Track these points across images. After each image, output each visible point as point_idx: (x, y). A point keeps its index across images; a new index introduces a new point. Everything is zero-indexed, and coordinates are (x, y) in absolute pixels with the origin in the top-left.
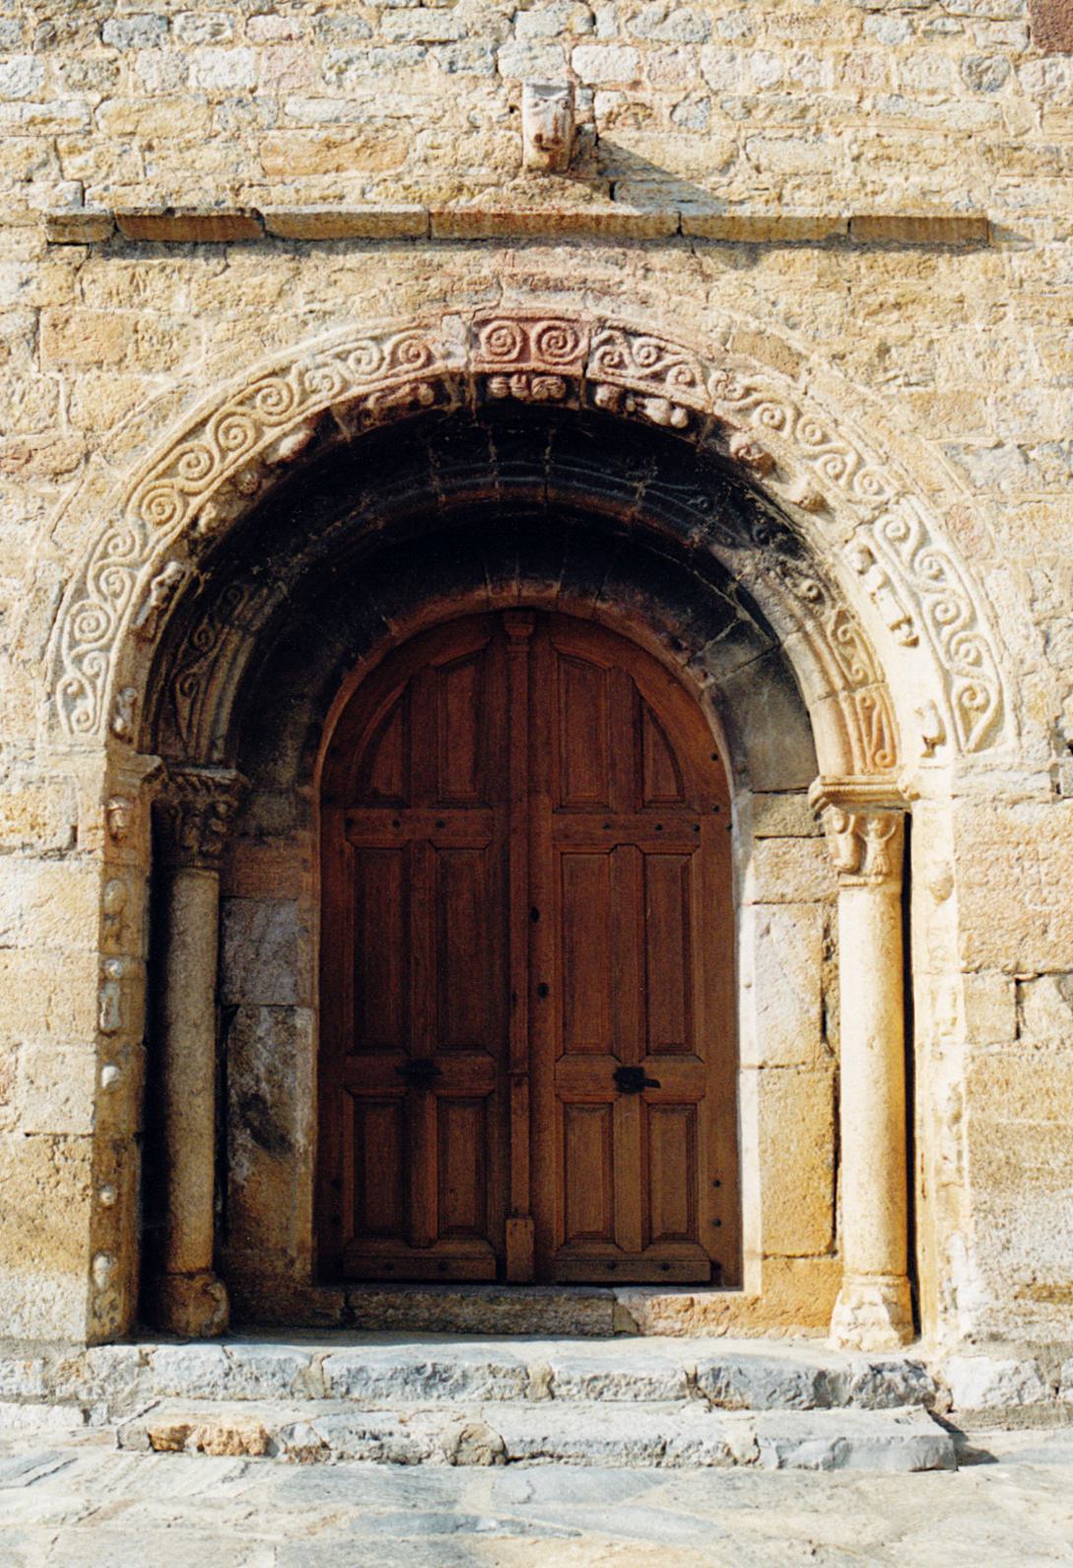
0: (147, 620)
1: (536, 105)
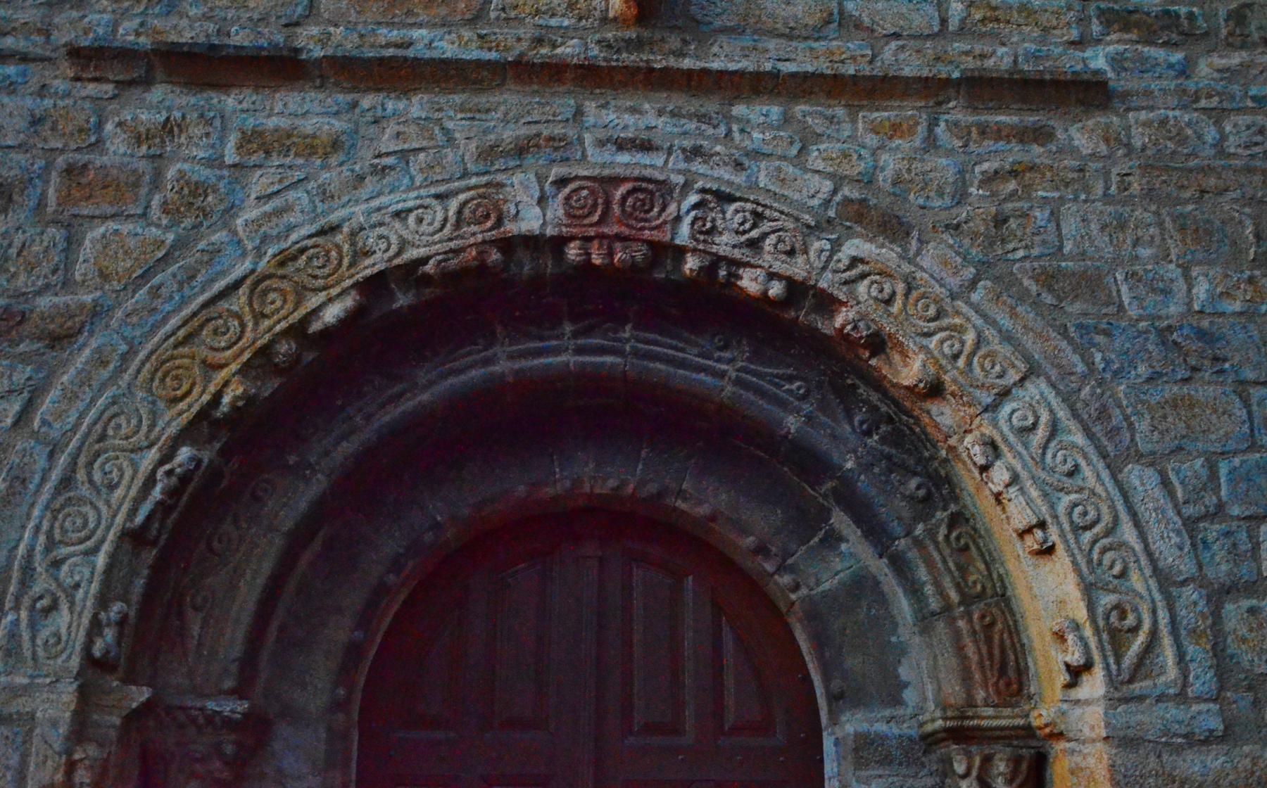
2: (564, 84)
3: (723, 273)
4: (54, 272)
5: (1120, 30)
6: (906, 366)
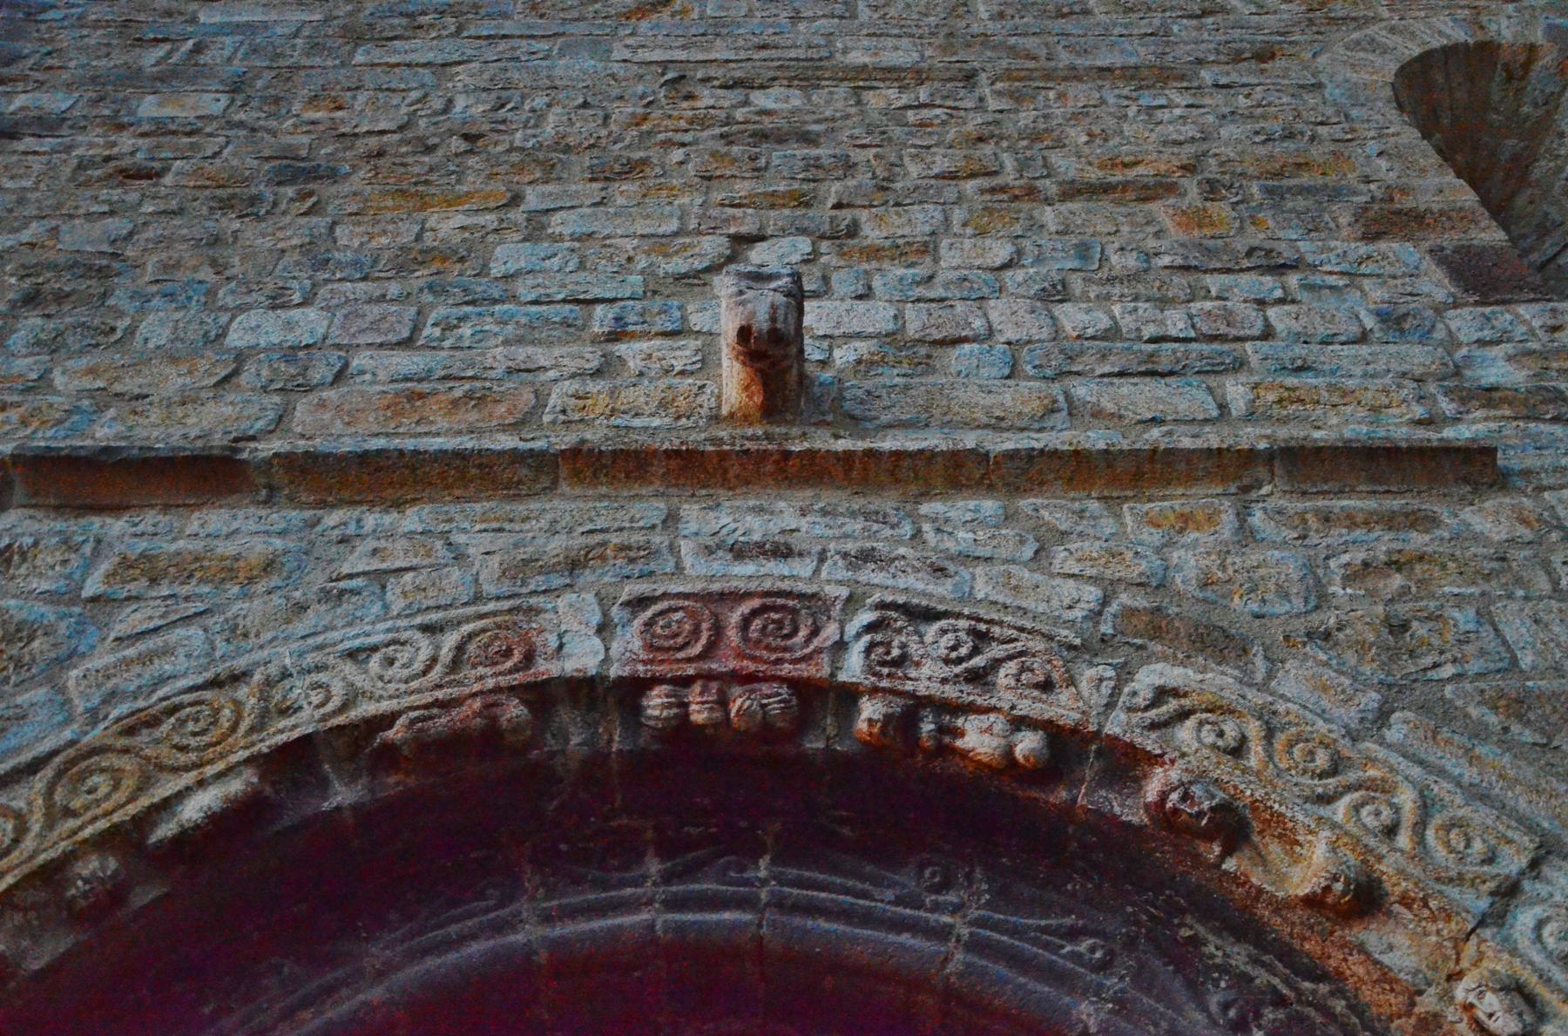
1: (741, 293)
2: (651, 483)
3: (927, 727)
5: (1484, 407)
6: (1296, 860)
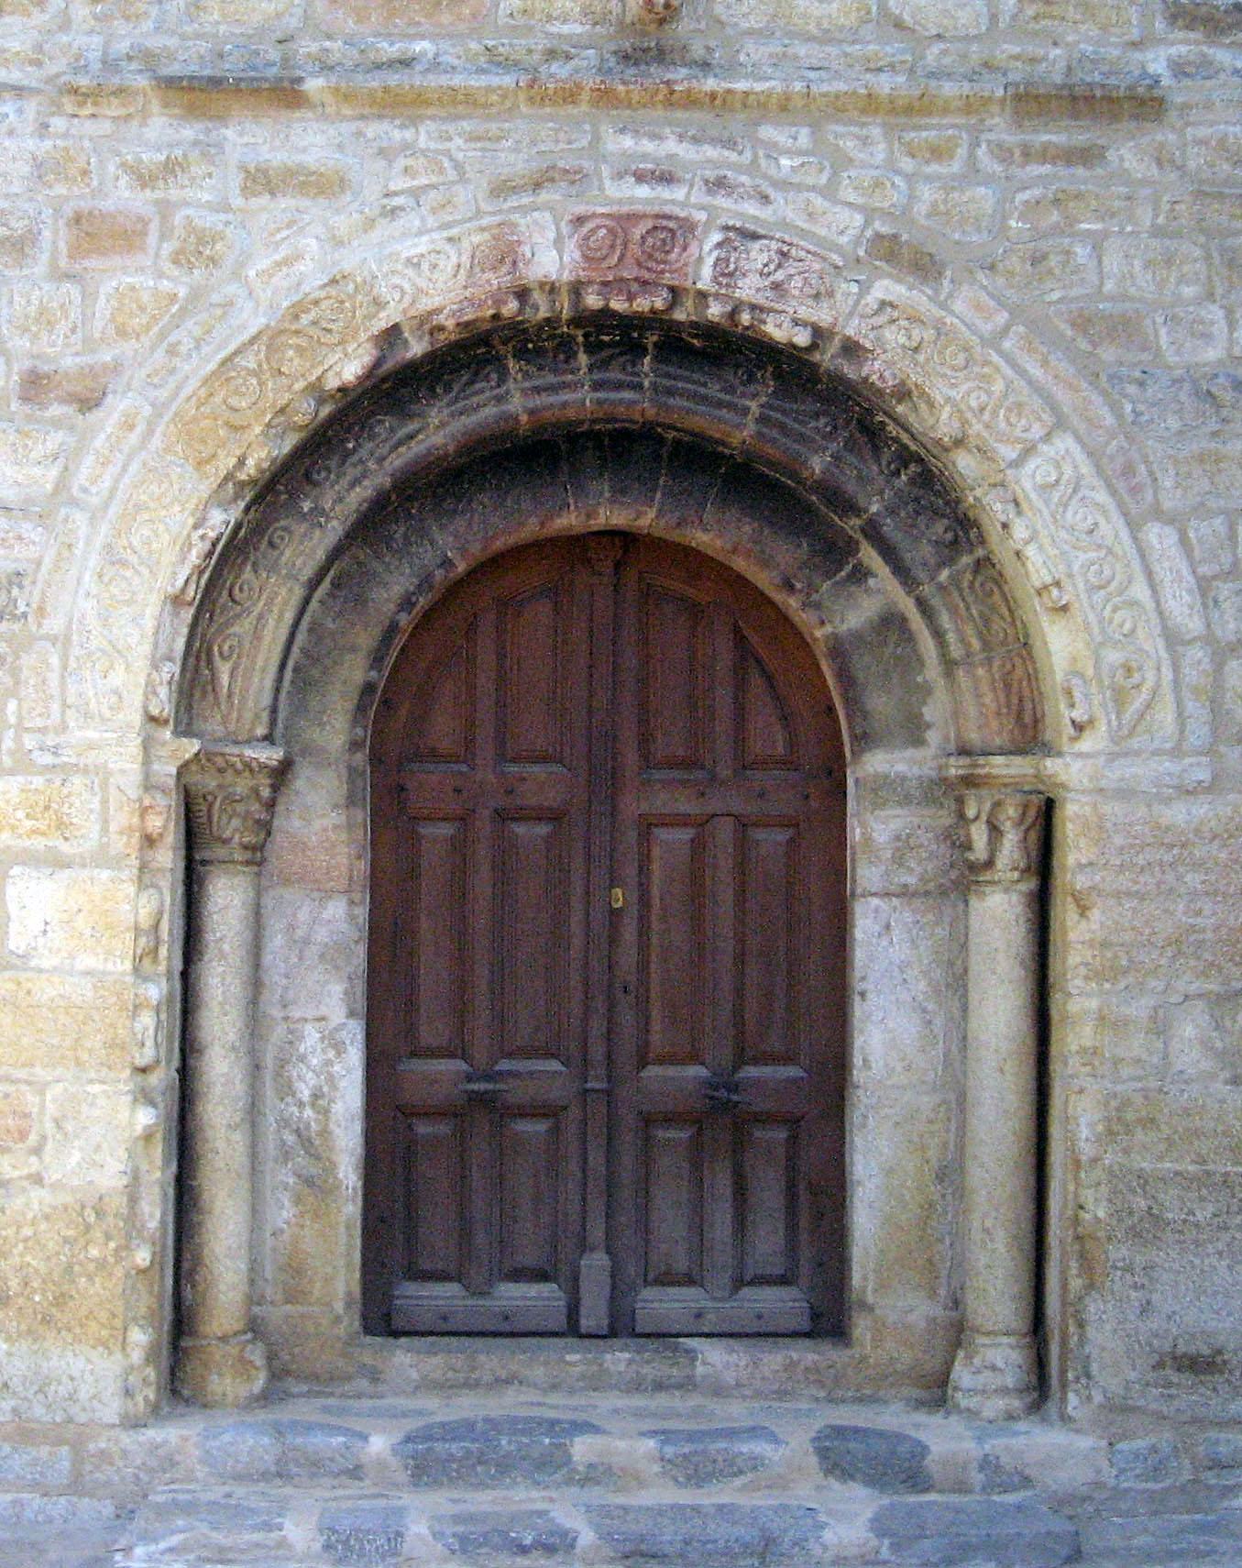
0: (187, 582)
4: (73, 331)
5: (1187, 27)
